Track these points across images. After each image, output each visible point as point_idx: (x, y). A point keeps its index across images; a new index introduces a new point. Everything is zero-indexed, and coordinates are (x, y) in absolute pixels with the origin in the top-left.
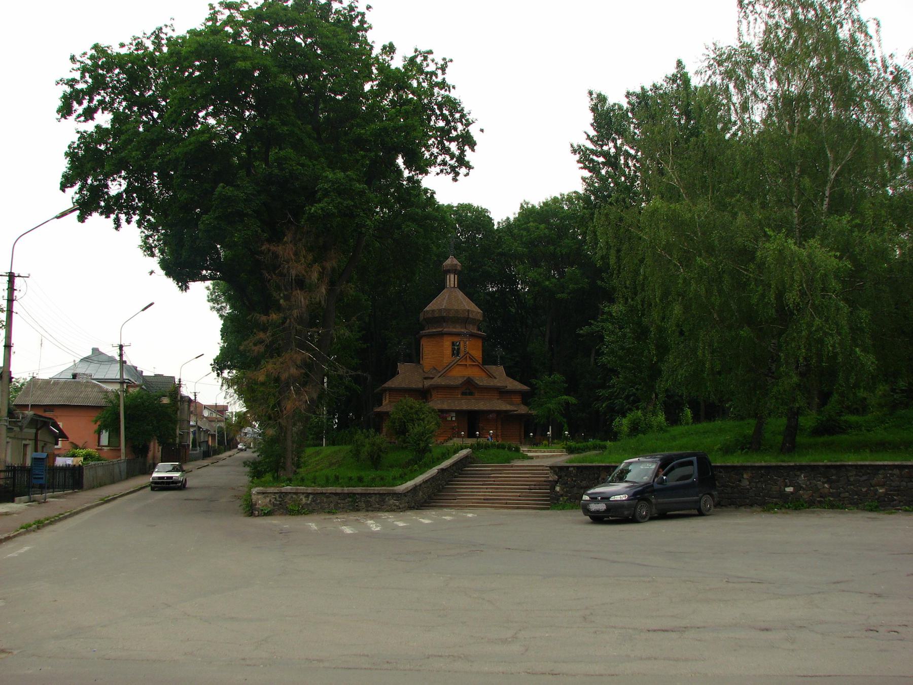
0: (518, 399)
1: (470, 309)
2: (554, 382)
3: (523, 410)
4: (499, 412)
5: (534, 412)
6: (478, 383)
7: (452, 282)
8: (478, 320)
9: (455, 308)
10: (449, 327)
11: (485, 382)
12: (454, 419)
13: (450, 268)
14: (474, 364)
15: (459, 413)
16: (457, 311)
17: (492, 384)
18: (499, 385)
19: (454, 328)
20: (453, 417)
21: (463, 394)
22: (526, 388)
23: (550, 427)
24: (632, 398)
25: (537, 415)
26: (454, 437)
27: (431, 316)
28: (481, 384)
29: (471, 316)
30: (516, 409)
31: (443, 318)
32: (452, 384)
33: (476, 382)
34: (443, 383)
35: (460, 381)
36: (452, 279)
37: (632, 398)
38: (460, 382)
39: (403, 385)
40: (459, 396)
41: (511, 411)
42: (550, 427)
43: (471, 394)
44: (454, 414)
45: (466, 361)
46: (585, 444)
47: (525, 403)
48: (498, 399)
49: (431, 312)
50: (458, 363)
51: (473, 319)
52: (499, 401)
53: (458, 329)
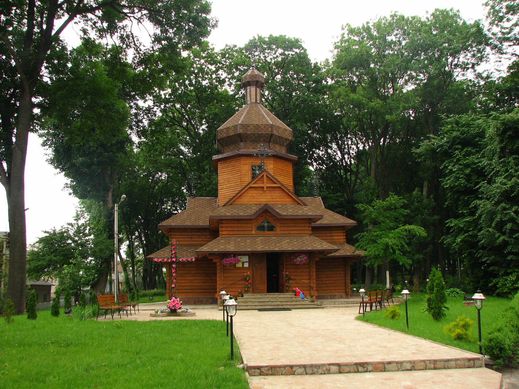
0: (341, 237)
1: (274, 124)
2: (389, 208)
3: (347, 250)
4: (310, 254)
5: (362, 253)
6: (280, 212)
7: (253, 97)
8: (286, 139)
9: (255, 123)
10: (248, 148)
11: (290, 210)
12: (246, 265)
13: (251, 80)
14: (275, 185)
15: (253, 256)
16: (257, 127)
17: (300, 213)
18: (310, 214)
19: (254, 148)
20: (244, 262)
21: (261, 228)
22: (350, 222)
23: (388, 273)
24: (509, 226)
25: (366, 257)
26: (246, 292)
27: (225, 135)
28: (284, 213)
29: (275, 132)
30: (335, 247)
31: (240, 135)
32: (242, 214)
33: (277, 210)
34: (228, 214)
35: (253, 210)
36: (253, 93)
37: (509, 226)
38: (254, 211)
39: (188, 223)
40: (254, 232)
41: (331, 251)
42: (388, 273)
43: (271, 228)
44: (245, 259)
45: (263, 183)
46: (115, 281)
47: (350, 241)
48: (310, 235)
49: (225, 131)
50: (251, 185)
51: (279, 137)
52: (312, 237)
53: (261, 148)
